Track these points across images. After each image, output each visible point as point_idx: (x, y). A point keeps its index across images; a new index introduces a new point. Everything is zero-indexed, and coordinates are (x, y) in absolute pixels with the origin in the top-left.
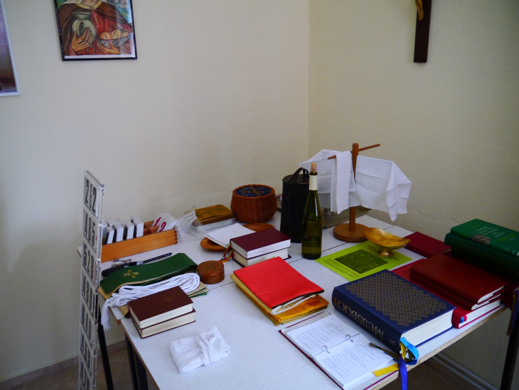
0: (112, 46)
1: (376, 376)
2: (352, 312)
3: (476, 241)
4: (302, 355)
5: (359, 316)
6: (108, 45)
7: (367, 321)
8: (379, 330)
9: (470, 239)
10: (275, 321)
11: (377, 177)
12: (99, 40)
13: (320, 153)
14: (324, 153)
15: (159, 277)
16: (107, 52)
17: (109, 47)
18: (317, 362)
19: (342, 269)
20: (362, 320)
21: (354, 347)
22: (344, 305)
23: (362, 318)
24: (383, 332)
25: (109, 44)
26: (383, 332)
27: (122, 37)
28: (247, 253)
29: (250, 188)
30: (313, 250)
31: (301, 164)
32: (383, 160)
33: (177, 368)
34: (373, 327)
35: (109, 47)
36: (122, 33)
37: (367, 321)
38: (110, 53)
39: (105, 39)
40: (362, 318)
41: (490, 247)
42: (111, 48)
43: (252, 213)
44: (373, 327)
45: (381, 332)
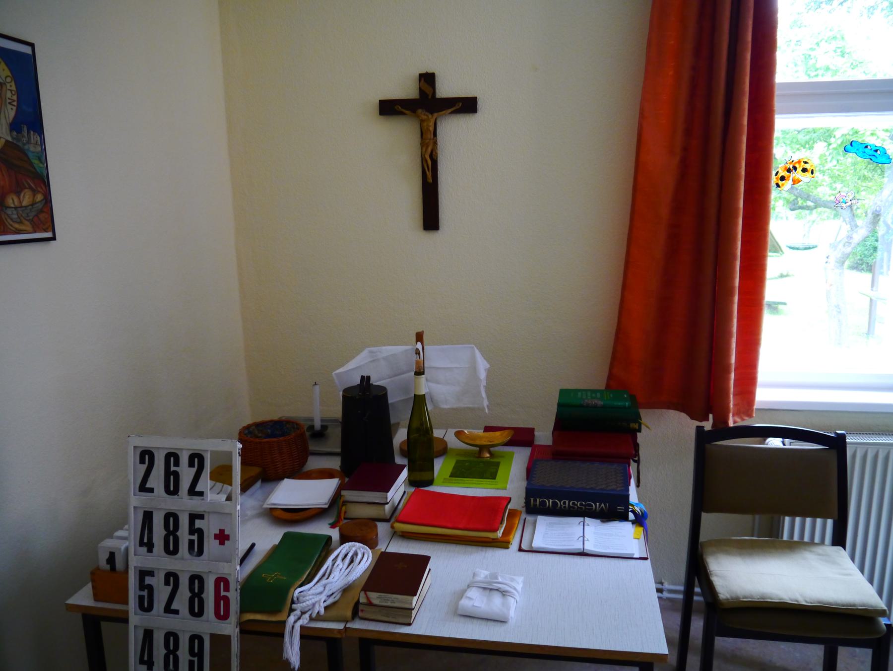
0: (22, 218)
1: (638, 539)
2: (560, 503)
3: (588, 406)
4: (567, 556)
5: (571, 503)
6: (15, 216)
7: (584, 503)
8: (603, 505)
9: (582, 406)
10: (503, 544)
11: (456, 368)
12: (4, 208)
13: (365, 353)
14: (371, 352)
15: (310, 569)
16: (16, 229)
17: (19, 220)
18: (590, 550)
19: (472, 482)
20: (577, 505)
21: (790, 445)
22: (546, 501)
23: (576, 503)
24: (607, 504)
25: (18, 215)
26: (607, 504)
27: (34, 202)
28: (387, 495)
29: (251, 429)
30: (424, 476)
31: (335, 374)
32: (461, 346)
33: (502, 621)
34: (593, 505)
35: (19, 220)
36: (34, 196)
37: (584, 503)
38: (19, 232)
39: (12, 206)
40: (576, 503)
41: (603, 407)
42: (21, 223)
43: (282, 459)
44: (593, 505)
45: (605, 506)
